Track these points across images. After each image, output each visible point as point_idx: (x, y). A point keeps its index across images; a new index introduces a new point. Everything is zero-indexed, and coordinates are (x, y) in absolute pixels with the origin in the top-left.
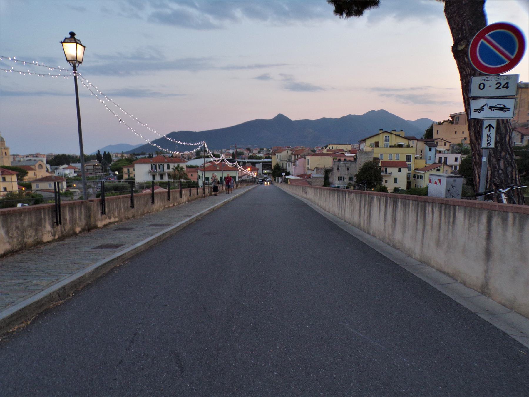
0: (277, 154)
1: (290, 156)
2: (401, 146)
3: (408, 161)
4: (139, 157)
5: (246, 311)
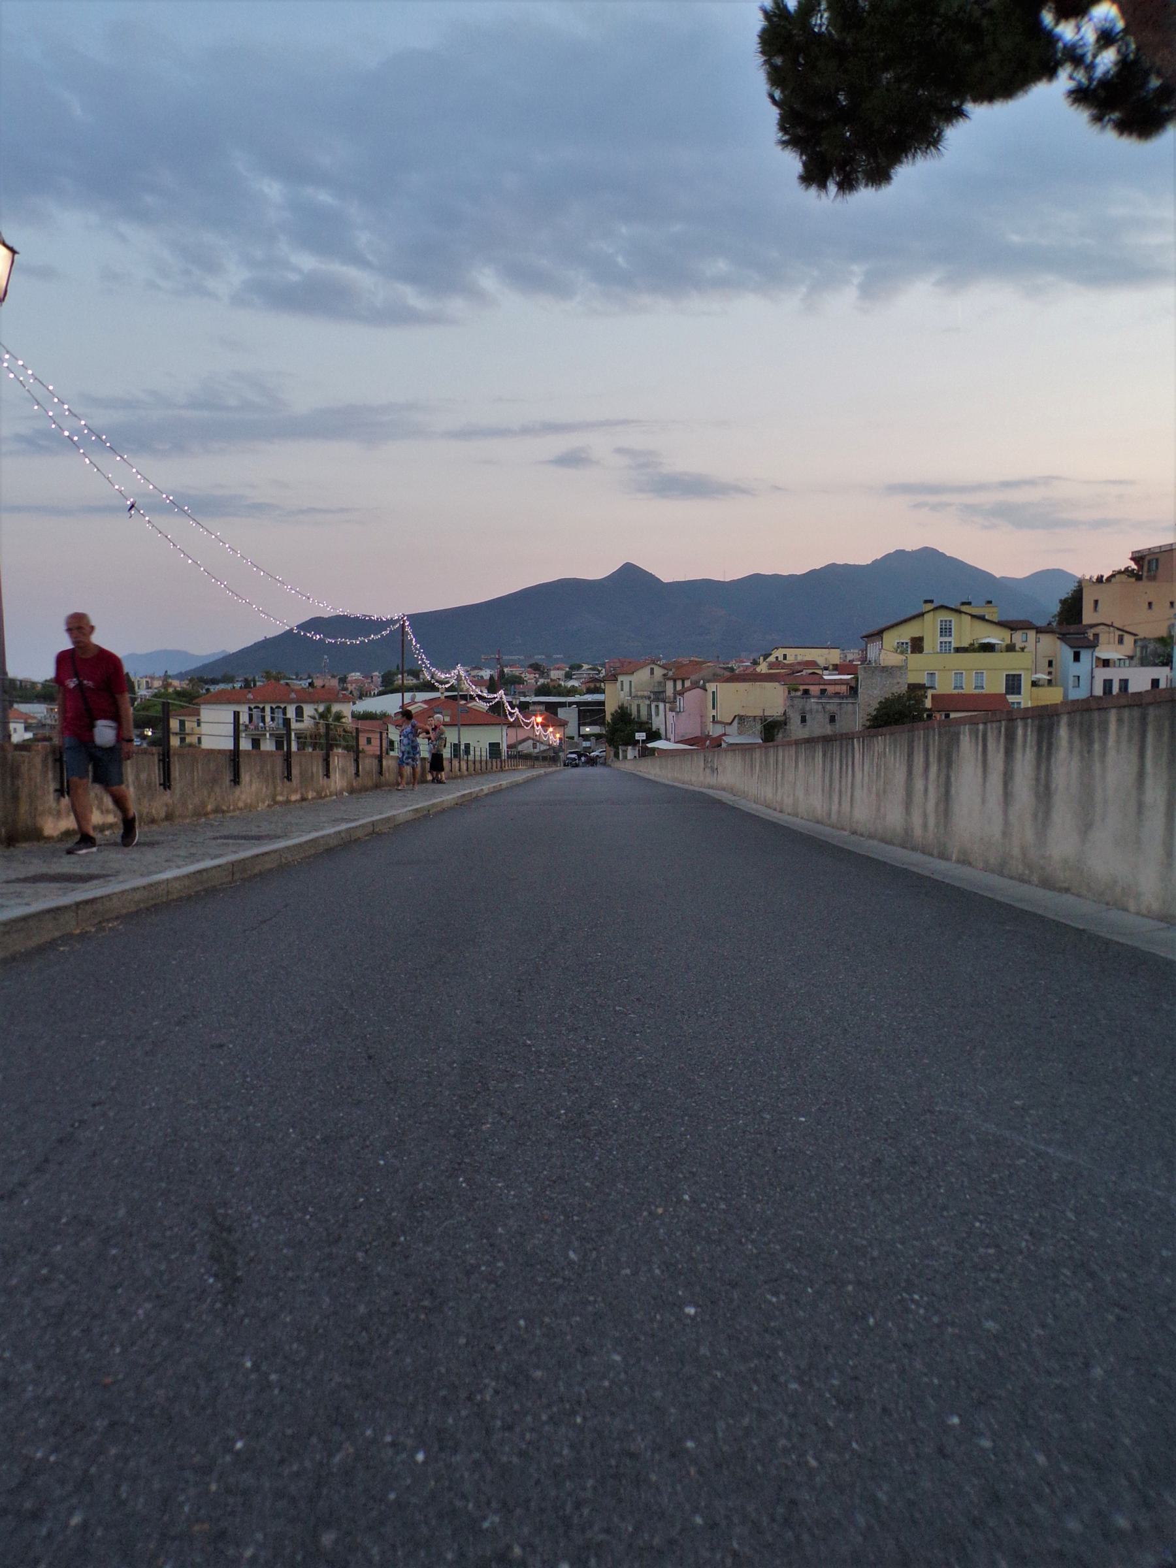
0: (620, 678)
1: (660, 683)
2: (988, 648)
3: (1013, 693)
4: (214, 688)
5: (540, 1067)
